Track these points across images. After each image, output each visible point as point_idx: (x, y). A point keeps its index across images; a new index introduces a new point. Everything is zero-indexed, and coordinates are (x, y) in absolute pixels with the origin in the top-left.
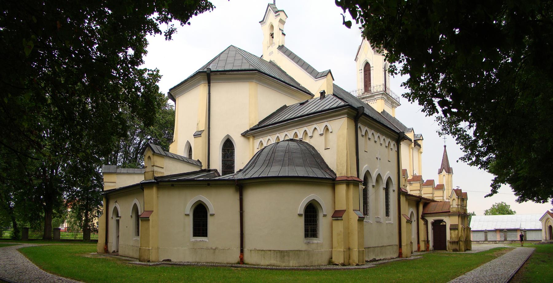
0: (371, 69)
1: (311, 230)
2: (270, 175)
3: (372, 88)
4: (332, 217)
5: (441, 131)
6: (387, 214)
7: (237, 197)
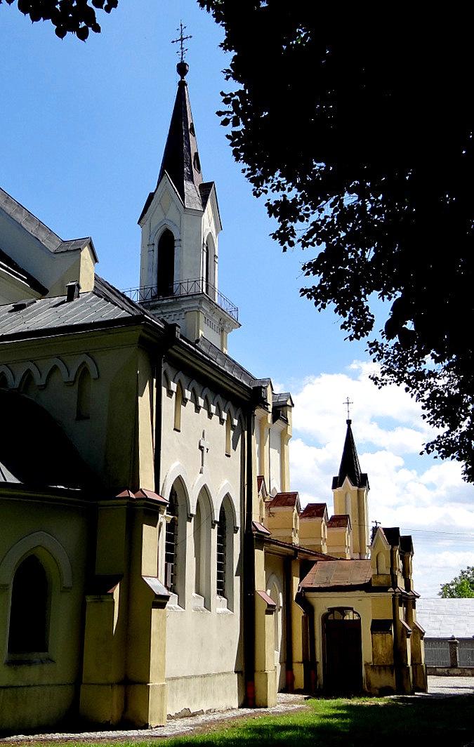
3: (175, 287)
5: (379, 376)
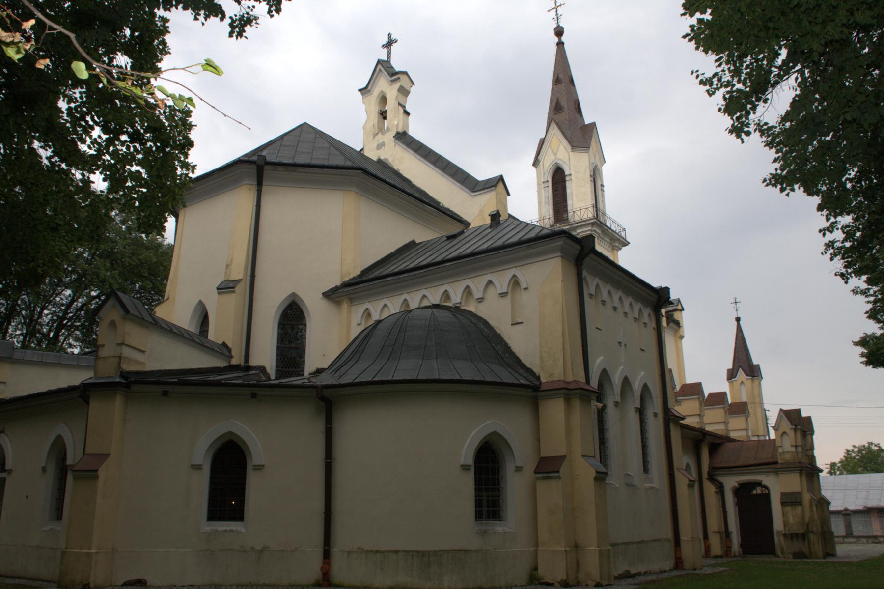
0: (567, 179)
1: (489, 503)
2: (398, 376)
3: (570, 215)
4: (536, 472)
5: (843, 271)
6: (646, 470)
7: (321, 426)
